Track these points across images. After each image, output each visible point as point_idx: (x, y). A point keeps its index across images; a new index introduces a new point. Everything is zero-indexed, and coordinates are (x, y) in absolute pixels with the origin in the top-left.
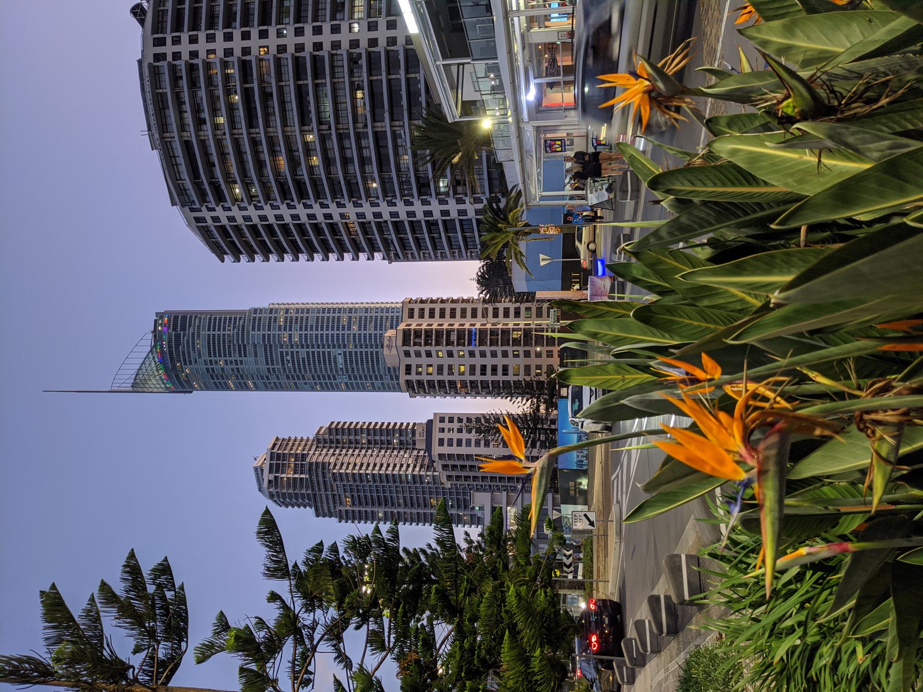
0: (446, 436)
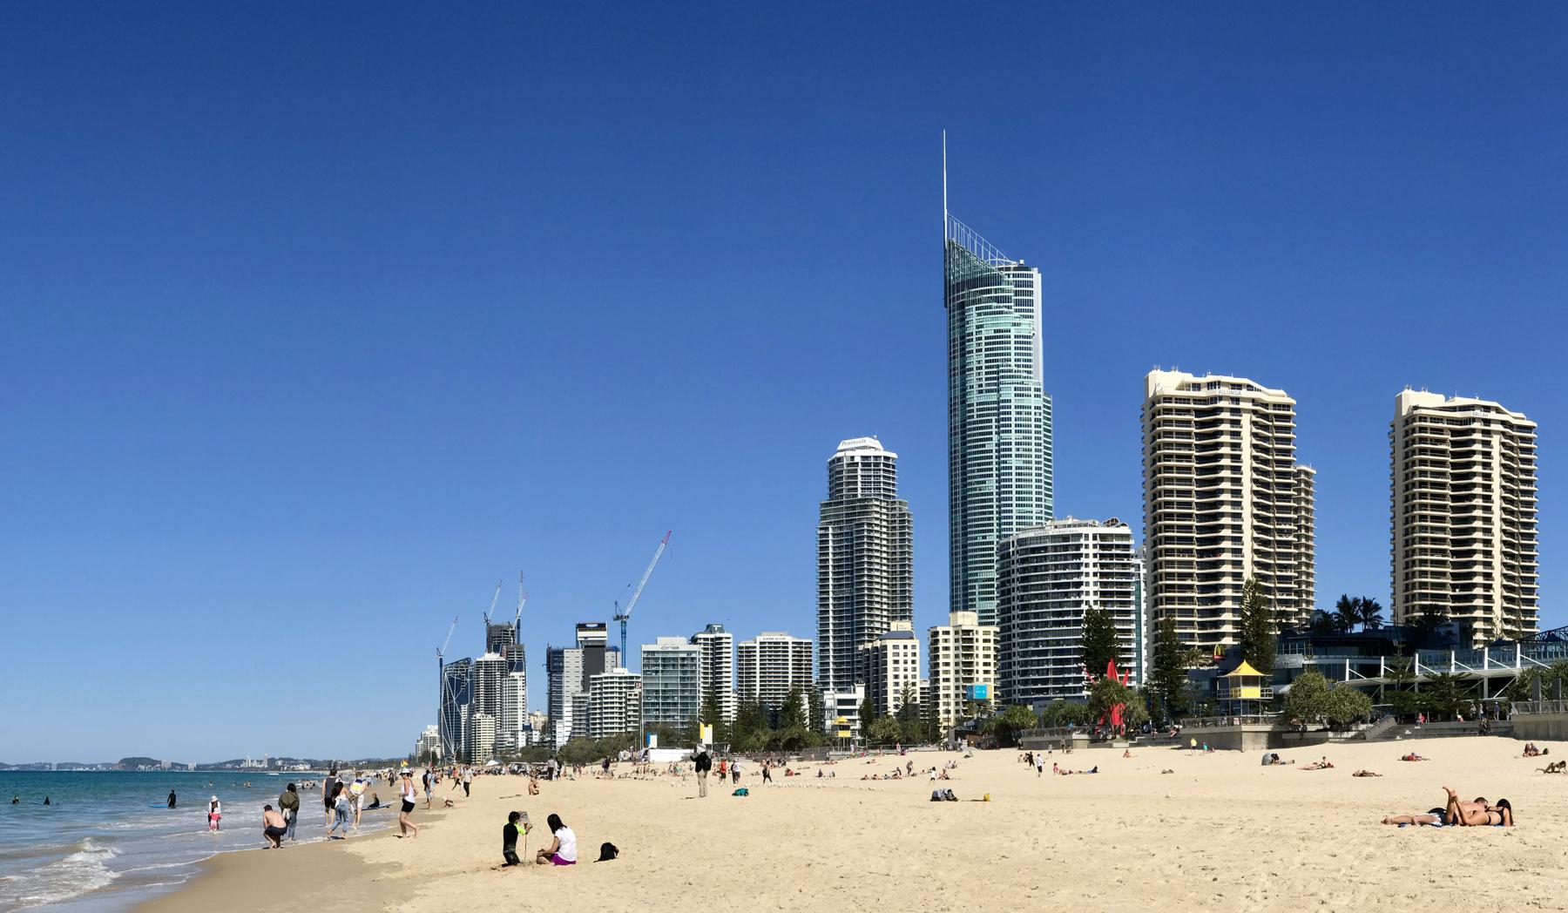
0: (901, 651)
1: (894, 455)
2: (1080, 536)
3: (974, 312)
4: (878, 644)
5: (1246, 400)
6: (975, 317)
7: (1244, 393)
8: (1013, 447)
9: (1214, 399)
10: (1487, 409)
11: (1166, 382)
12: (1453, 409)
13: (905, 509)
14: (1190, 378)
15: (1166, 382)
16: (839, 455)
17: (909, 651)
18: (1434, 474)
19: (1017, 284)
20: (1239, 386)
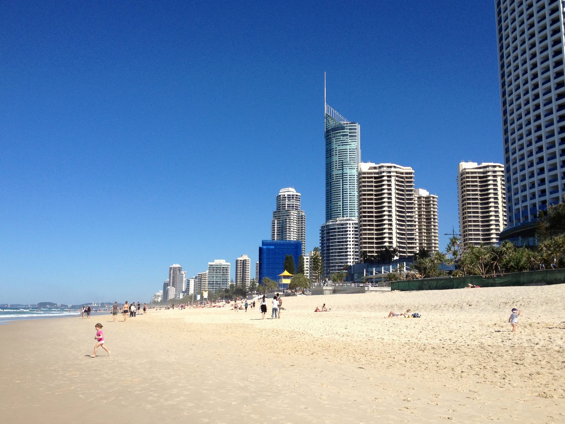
1: (299, 194)
2: (347, 224)
3: (334, 141)
5: (393, 172)
6: (335, 143)
7: (393, 169)
8: (348, 190)
10: (494, 166)
11: (469, 166)
12: (480, 168)
13: (303, 214)
14: (374, 165)
15: (469, 166)
16: (280, 194)
18: (473, 195)
19: (350, 129)
20: (391, 167)
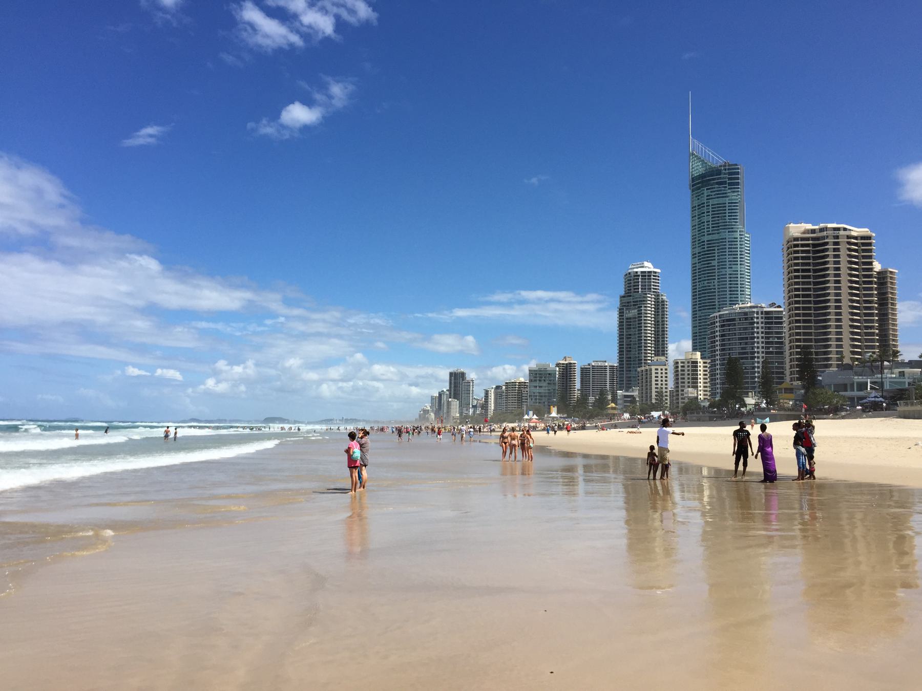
0: (659, 371)
4: (647, 367)
9: (823, 238)
14: (810, 226)
17: (664, 371)
20: (838, 229)
